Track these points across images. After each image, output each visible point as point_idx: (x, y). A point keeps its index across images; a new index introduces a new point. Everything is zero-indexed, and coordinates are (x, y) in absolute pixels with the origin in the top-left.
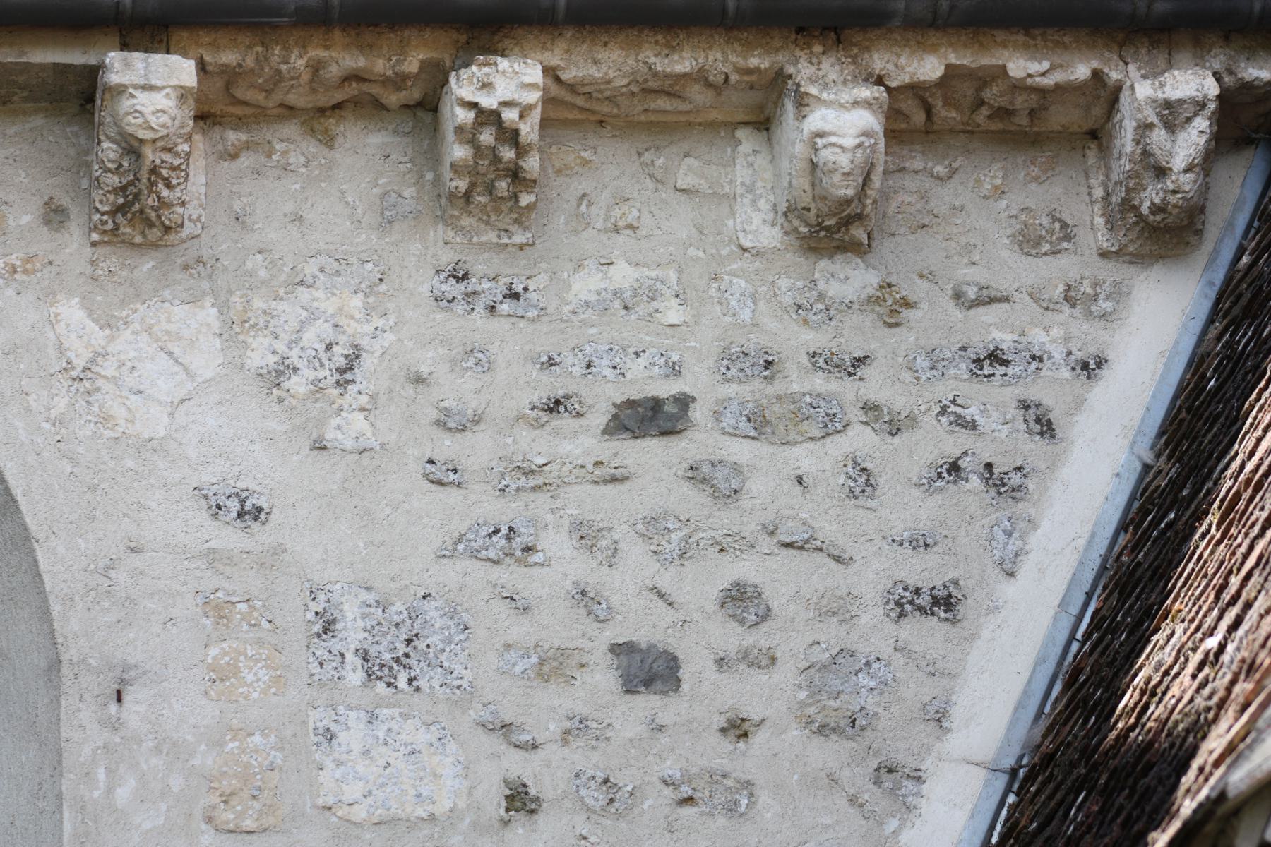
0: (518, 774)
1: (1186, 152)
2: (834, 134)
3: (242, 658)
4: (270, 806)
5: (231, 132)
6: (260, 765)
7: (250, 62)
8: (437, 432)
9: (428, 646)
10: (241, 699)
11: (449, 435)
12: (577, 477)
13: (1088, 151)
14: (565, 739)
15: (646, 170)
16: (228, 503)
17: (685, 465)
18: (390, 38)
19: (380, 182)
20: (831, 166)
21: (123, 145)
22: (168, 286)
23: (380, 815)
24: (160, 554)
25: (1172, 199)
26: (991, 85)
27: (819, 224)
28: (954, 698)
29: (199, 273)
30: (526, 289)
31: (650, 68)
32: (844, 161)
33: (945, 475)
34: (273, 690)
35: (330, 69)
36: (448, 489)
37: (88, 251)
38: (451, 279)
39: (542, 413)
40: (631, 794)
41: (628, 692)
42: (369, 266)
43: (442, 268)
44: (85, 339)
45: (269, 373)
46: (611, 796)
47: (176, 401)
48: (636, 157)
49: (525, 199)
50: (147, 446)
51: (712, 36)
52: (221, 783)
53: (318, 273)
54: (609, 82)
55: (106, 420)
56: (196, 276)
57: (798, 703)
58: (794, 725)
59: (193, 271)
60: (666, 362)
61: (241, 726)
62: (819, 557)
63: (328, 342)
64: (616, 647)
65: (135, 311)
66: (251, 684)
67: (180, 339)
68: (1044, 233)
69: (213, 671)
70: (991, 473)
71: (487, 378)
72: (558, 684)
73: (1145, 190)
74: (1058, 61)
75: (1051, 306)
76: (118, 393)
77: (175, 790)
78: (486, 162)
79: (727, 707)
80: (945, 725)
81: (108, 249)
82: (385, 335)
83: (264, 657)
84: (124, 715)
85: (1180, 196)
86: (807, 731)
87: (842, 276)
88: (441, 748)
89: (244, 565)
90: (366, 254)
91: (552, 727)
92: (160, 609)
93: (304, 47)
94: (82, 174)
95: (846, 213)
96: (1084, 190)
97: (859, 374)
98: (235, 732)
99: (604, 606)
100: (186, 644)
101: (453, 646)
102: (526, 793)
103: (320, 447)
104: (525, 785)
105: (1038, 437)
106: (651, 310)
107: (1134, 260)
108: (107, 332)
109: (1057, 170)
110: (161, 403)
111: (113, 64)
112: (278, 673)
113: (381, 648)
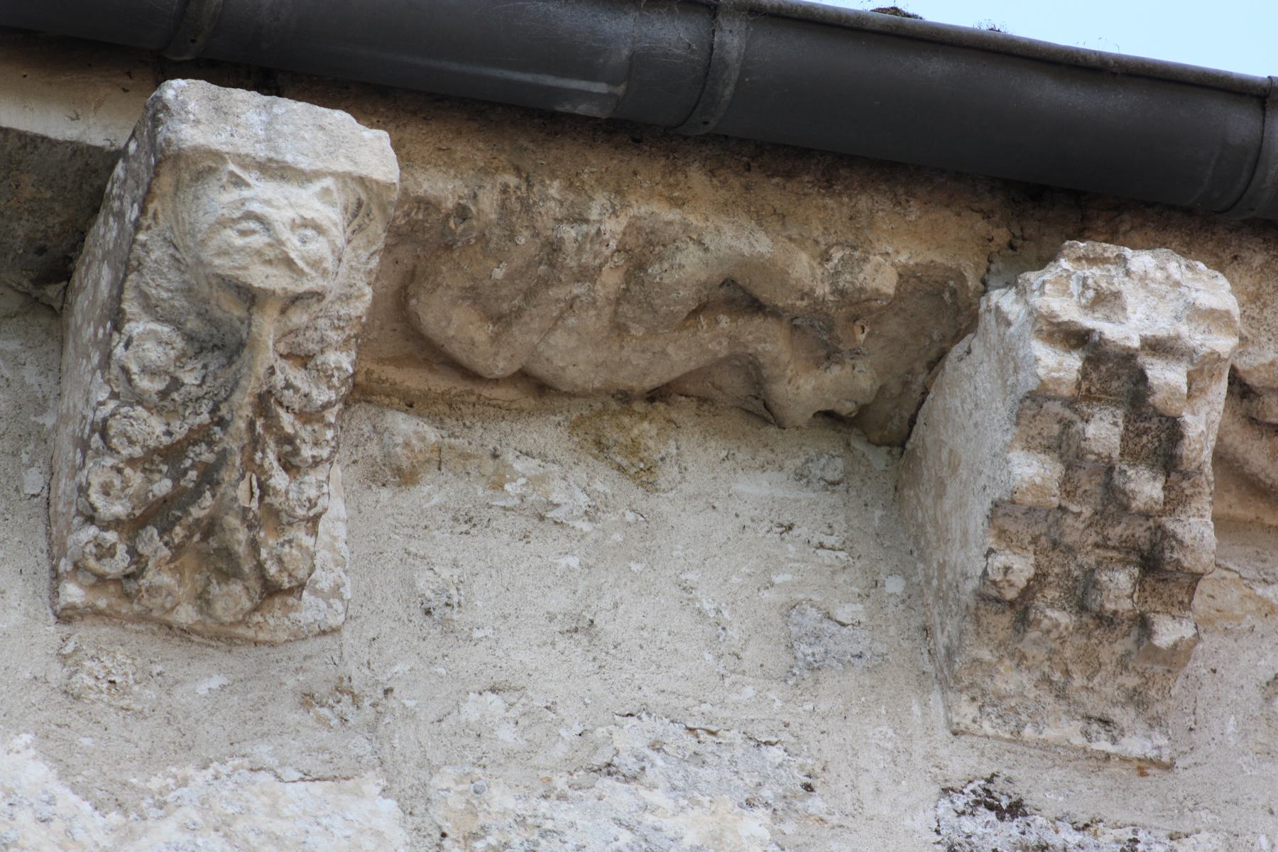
5: (401, 417)
7: (488, 203)
18: (825, 207)
19: (778, 579)
21: (192, 324)
22: (264, 735)
29: (344, 720)
35: (680, 258)
37: (51, 631)
38: (982, 809)
42: (776, 754)
43: (957, 786)
44: (58, 825)
53: (648, 752)
56: (335, 722)
59: (325, 712)
65: (184, 782)
78: (1087, 512)
81: (105, 632)
90: (762, 728)
93: (618, 192)
94: (25, 458)
108: (115, 817)
111: (184, 103)
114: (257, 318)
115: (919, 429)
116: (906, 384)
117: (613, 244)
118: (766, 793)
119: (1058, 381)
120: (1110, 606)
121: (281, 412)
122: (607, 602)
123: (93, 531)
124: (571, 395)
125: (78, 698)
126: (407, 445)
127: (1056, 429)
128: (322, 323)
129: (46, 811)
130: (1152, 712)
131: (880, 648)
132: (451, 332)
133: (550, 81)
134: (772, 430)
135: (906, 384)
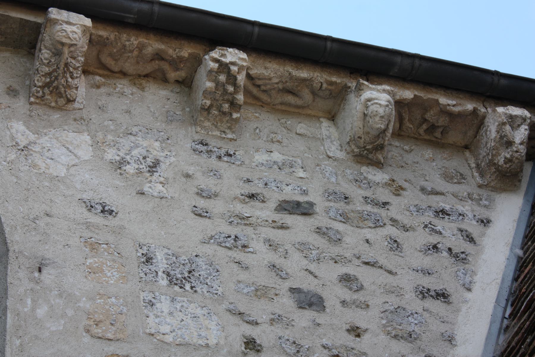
0: (250, 334)
1: (520, 137)
2: (377, 99)
3: (105, 266)
4: (121, 330)
6: (115, 312)
7: (112, 37)
8: (198, 198)
9: (200, 275)
10: (104, 282)
11: (203, 199)
12: (265, 224)
13: (465, 153)
14: (272, 323)
15: (283, 126)
16: (96, 206)
17: (316, 227)
19: (166, 107)
20: (375, 113)
21: (53, 50)
23: (180, 341)
24: (62, 220)
25: (516, 155)
26: (430, 111)
27: (364, 147)
28: (455, 332)
29: (82, 123)
30: (234, 154)
31: (290, 74)
32: (381, 111)
33: (431, 249)
34: (121, 281)
35: (148, 49)
36: (204, 219)
37: (28, 106)
39: (246, 198)
40: (308, 350)
41: (301, 307)
42: (162, 133)
44: (25, 136)
45: (116, 162)
46: (298, 349)
47: (70, 165)
48: (278, 121)
49: (235, 115)
50: (54, 179)
51: (315, 68)
52: (94, 316)
54: (270, 79)
55: (35, 166)
56: (80, 124)
57: (382, 325)
58: (382, 334)
59: (78, 122)
60: (301, 189)
61: (104, 293)
62: (380, 270)
63: (144, 156)
64: (292, 290)
65: (51, 131)
66: (110, 277)
67: (72, 144)
68: (454, 175)
69: (90, 268)
70: (452, 253)
71: (220, 181)
72: (265, 300)
73: (500, 155)
74: (459, 102)
75: (463, 199)
76: (41, 157)
77: (69, 315)
78: (220, 93)
79: (349, 322)
80: (454, 343)
81: (38, 106)
82: (171, 158)
83: (116, 267)
84: (42, 278)
85: (519, 154)
86: (389, 336)
87: (373, 174)
88: (209, 317)
89: (104, 231)
91: (264, 317)
92: (62, 240)
93: (137, 37)
94: (26, 79)
95: (376, 143)
96: (467, 165)
97: (387, 207)
98: (101, 296)
99: (284, 272)
100: (75, 256)
101: (212, 277)
102: (255, 342)
103: (142, 193)
104: (253, 339)
105: (468, 243)
106: (291, 171)
107: (493, 190)
108: (36, 136)
109: (454, 157)
110: (63, 165)
112: (124, 275)
113: (176, 272)
114: (64, 48)
115: (193, 83)
116: (191, 76)
117: (136, 46)
118: (160, 139)
119: (214, 68)
120: (224, 110)
121: (70, 68)
122: (134, 108)
123: (35, 88)
124: (130, 76)
125: (32, 117)
126: (98, 81)
127: (214, 78)
128: (77, 51)
129: (23, 134)
130: (233, 130)
131: (184, 119)
132: (107, 62)
133: (123, 14)
134: (167, 83)
135: (191, 76)
